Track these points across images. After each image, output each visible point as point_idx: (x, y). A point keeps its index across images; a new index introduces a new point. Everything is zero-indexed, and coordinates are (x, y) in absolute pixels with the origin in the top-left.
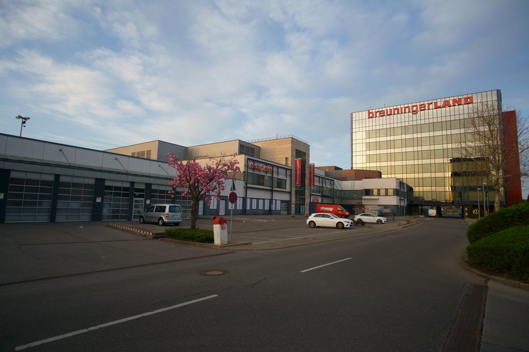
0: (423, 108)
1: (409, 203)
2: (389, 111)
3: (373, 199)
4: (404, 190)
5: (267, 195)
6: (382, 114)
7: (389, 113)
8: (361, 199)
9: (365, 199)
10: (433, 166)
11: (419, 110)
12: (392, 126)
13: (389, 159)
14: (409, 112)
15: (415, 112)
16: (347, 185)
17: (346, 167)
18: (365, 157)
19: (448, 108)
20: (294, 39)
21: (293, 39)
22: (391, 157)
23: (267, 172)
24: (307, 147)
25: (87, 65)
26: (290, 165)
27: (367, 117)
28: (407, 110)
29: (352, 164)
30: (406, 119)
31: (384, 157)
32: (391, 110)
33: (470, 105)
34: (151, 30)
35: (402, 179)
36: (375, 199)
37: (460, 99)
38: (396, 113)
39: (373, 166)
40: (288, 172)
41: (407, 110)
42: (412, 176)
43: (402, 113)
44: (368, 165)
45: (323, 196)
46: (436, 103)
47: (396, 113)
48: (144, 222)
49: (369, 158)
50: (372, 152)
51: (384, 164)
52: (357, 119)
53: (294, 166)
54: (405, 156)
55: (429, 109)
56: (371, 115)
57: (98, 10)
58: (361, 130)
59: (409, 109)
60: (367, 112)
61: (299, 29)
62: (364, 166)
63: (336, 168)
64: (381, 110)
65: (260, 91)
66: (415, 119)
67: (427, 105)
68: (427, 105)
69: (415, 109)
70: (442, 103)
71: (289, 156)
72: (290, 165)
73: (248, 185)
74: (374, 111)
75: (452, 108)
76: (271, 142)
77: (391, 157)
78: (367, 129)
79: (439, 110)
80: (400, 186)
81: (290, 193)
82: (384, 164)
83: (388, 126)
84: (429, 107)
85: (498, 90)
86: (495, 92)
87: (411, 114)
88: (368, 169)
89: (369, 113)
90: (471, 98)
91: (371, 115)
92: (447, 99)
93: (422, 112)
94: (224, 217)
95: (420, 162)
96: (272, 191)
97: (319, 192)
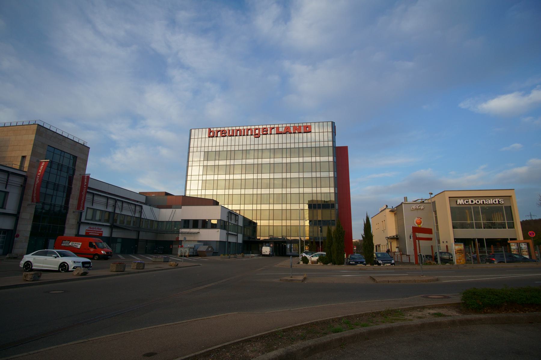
0: (265, 132)
1: (246, 239)
3: (191, 233)
4: (231, 221)
6: (224, 134)
8: (178, 233)
9: (182, 233)
10: (272, 196)
11: (261, 133)
12: (233, 149)
14: (251, 135)
15: (257, 136)
17: (177, 192)
18: (200, 182)
19: (289, 135)
21: (176, 74)
22: (231, 184)
26: (26, 169)
27: (207, 136)
29: (186, 190)
31: (222, 184)
32: (233, 130)
33: (309, 134)
35: (240, 210)
36: (194, 233)
37: (300, 127)
39: (208, 194)
40: (18, 181)
42: (249, 207)
43: (244, 135)
44: (203, 192)
45: (112, 227)
46: (278, 128)
54: (244, 184)
55: (271, 134)
56: (212, 134)
58: (199, 149)
59: (252, 132)
61: (182, 66)
62: (199, 193)
63: (167, 194)
64: (222, 129)
65: (135, 120)
66: (256, 143)
67: (269, 129)
68: (269, 129)
69: (257, 132)
70: (284, 128)
71: (28, 153)
72: (26, 169)
73: (229, 232)
74: (215, 129)
75: (293, 135)
76: (5, 129)
77: (231, 184)
78: (206, 150)
79: (280, 135)
80: (228, 217)
81: (16, 216)
83: (229, 149)
84: (271, 131)
85: (332, 122)
86: (330, 124)
87: (253, 137)
88: (203, 197)
89: (210, 131)
90: (310, 127)
91: (211, 134)
92: (288, 125)
95: (259, 191)
97: (108, 221)
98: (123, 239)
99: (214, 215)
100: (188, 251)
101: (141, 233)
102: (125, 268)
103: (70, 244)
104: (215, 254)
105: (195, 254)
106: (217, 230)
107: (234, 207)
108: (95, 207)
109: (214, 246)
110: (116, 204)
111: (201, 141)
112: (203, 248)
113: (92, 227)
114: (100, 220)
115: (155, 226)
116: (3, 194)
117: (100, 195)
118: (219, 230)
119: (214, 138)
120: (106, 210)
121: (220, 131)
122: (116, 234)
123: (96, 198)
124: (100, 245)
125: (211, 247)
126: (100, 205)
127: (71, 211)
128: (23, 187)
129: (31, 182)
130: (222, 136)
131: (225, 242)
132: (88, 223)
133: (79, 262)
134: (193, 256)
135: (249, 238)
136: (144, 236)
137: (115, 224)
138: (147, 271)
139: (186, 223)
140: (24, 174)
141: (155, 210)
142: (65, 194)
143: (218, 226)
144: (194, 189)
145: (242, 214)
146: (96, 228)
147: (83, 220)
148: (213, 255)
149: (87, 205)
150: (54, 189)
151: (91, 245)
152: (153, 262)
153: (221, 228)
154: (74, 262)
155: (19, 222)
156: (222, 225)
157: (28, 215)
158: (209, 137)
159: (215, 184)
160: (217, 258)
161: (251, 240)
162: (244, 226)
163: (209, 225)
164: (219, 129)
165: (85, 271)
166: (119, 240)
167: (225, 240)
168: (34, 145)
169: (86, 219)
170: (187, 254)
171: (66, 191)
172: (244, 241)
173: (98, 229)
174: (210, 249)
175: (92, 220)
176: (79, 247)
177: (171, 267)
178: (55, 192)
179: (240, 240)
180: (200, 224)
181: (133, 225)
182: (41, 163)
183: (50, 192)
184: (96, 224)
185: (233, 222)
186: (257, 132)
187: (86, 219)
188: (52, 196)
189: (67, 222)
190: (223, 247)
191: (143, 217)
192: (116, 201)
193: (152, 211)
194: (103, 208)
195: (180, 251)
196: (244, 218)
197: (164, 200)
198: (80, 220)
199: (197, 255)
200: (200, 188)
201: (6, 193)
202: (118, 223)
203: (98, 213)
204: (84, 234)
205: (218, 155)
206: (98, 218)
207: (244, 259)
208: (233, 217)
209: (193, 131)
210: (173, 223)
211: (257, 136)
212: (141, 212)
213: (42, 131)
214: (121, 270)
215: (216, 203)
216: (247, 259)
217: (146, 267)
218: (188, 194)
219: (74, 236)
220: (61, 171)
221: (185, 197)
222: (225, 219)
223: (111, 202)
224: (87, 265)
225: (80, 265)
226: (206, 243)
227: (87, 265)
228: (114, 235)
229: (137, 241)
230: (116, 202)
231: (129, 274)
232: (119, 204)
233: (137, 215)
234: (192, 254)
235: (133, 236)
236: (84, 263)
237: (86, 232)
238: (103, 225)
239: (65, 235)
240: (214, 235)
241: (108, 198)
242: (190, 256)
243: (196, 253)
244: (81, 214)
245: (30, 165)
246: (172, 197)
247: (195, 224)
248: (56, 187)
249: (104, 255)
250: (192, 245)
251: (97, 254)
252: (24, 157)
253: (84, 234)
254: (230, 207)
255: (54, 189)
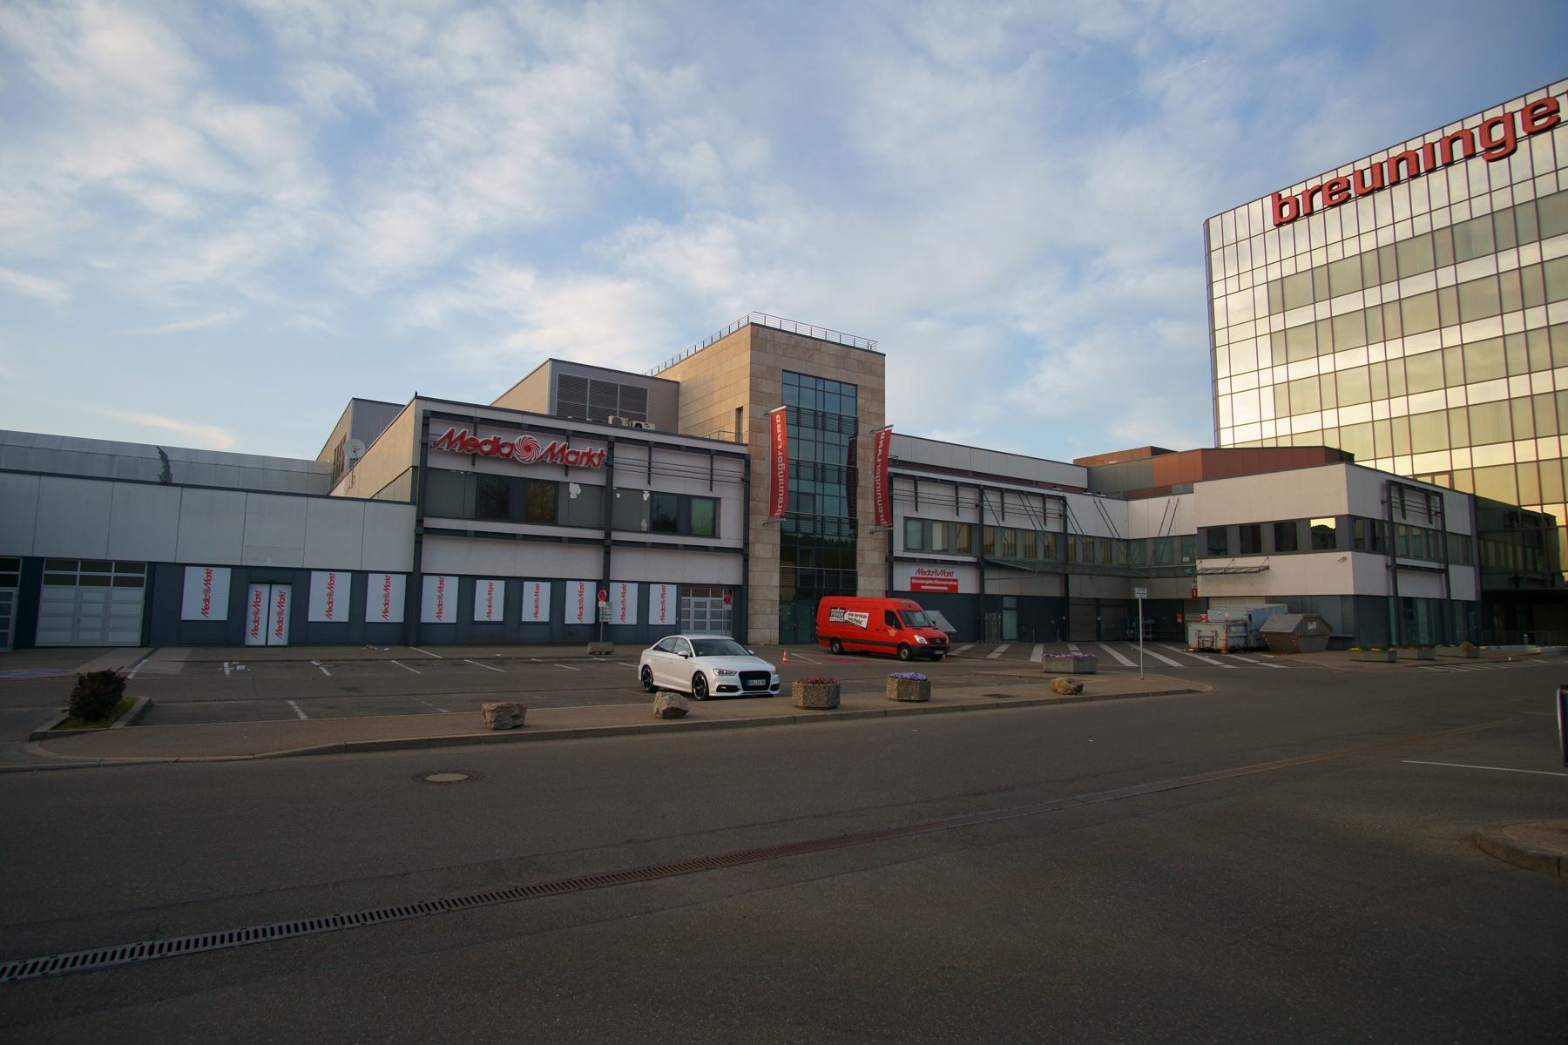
1: (1499, 584)
2: (1367, 174)
3: (1237, 572)
4: (1397, 517)
5: (586, 564)
6: (1337, 193)
7: (1368, 183)
8: (1194, 574)
11: (1520, 133)
13: (1380, 391)
16: (1149, 517)
17: (1181, 442)
18: (1267, 393)
20: (1170, 82)
23: (567, 468)
24: (872, 362)
25: (609, 269)
28: (1458, 150)
29: (1217, 430)
30: (1464, 189)
34: (752, 151)
35: (1450, 473)
36: (1248, 572)
38: (1404, 174)
39: (1305, 429)
40: (733, 469)
41: (1458, 150)
43: (1433, 170)
44: (1284, 427)
45: (983, 566)
47: (1404, 174)
48: (842, 652)
49: (1287, 398)
50: (1300, 370)
51: (1355, 414)
52: (1230, 238)
53: (765, 440)
57: (625, 130)
58: (1246, 281)
60: (1268, 202)
61: (1183, 46)
62: (1269, 431)
63: (1156, 451)
64: (1327, 179)
65: (1074, 263)
69: (1498, 133)
71: (744, 400)
72: (745, 440)
73: (1400, 561)
74: (1297, 190)
78: (1274, 274)
80: (1387, 503)
81: (743, 553)
82: (1355, 414)
89: (1279, 203)
91: (1286, 211)
93: (1537, 140)
94: (132, 668)
96: (607, 547)
98: (1019, 598)
99: (1320, 499)
100: (1222, 635)
101: (1074, 581)
102: (838, 698)
103: (846, 617)
104: (1338, 643)
105: (1253, 643)
106: (1340, 555)
107: (1424, 464)
108: (925, 513)
109: (1334, 619)
110: (981, 500)
111: (1262, 256)
112: (1284, 623)
113: (926, 569)
114: (945, 551)
115: (1119, 558)
116: (710, 504)
117: (935, 480)
118: (1348, 554)
119: (1301, 224)
120: (915, 515)
121: (1319, 189)
122: (996, 585)
123: (924, 489)
124: (918, 617)
125: (1320, 619)
126: (937, 506)
127: (863, 531)
128: (746, 482)
129: (762, 467)
130: (1333, 206)
131: (1384, 600)
132: (914, 560)
133: (729, 673)
134: (1247, 650)
135: (1516, 579)
136: (1082, 587)
137: (987, 557)
138: (934, 711)
139: (1216, 540)
140: (743, 450)
141: (1114, 506)
142: (844, 488)
143: (1343, 538)
144: (1246, 423)
145: (1463, 485)
146: (937, 572)
147: (899, 551)
148: (1329, 648)
149: (901, 510)
150: (815, 480)
151: (890, 618)
152: (1129, 672)
153: (1357, 546)
154: (721, 672)
155: (752, 567)
156: (1360, 534)
157: (767, 549)
158: (1279, 225)
159: (1330, 392)
160: (1334, 661)
161: (1523, 587)
162: (1481, 533)
163: (1304, 538)
164: (1311, 185)
165: (676, 704)
166: (1008, 603)
167: (1383, 593)
168: (752, 376)
169: (906, 549)
170: (1220, 644)
171: (844, 480)
172: (1488, 596)
173: (943, 573)
174: (1312, 626)
175: (922, 550)
176: (864, 625)
177: (1057, 696)
178: (819, 485)
179: (1464, 584)
180: (1268, 538)
181: (1046, 556)
182: (773, 417)
183: (806, 487)
184: (935, 561)
185: (1416, 519)
186: (1498, 133)
187: (906, 549)
188: (814, 495)
189: (859, 560)
190: (1374, 621)
191: (1071, 530)
192: (981, 490)
193: (1103, 514)
194: (948, 515)
195: (1196, 632)
196: (1477, 503)
197: (1155, 472)
198: (891, 552)
199: (1265, 649)
200: (1268, 413)
201: (716, 501)
202: (998, 554)
203: (937, 531)
204: (908, 588)
205: (1323, 283)
206: (938, 543)
207: (1474, 668)
208: (1413, 501)
209: (1215, 224)
210: (1177, 545)
211: (1502, 151)
212: (1064, 517)
213: (762, 337)
214: (823, 703)
215: (1348, 458)
216: (1490, 667)
217: (935, 693)
218: (1227, 441)
219: (881, 595)
220: (823, 429)
221: (1218, 452)
222: (1375, 511)
223: (968, 496)
224: (755, 682)
225: (735, 680)
226: (1295, 604)
227: (755, 682)
228: (992, 588)
229: (1063, 603)
230: (981, 495)
231: (1091, 699)
232: (992, 499)
233: (1054, 526)
234: (1241, 643)
235: (1051, 588)
236: (745, 676)
237: (913, 585)
238: (955, 563)
239: (859, 594)
240: (1331, 575)
241: (956, 485)
242: (1232, 650)
243: (1255, 642)
244: (891, 534)
245: (753, 428)
246: (1169, 457)
247: (1251, 538)
248: (820, 472)
249: (922, 646)
250: (1239, 612)
251: (903, 645)
252: (740, 410)
253: (908, 588)
254: (1403, 468)
255: (815, 480)
